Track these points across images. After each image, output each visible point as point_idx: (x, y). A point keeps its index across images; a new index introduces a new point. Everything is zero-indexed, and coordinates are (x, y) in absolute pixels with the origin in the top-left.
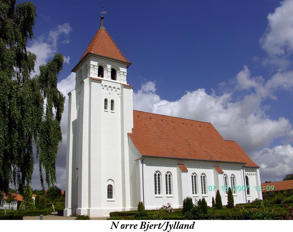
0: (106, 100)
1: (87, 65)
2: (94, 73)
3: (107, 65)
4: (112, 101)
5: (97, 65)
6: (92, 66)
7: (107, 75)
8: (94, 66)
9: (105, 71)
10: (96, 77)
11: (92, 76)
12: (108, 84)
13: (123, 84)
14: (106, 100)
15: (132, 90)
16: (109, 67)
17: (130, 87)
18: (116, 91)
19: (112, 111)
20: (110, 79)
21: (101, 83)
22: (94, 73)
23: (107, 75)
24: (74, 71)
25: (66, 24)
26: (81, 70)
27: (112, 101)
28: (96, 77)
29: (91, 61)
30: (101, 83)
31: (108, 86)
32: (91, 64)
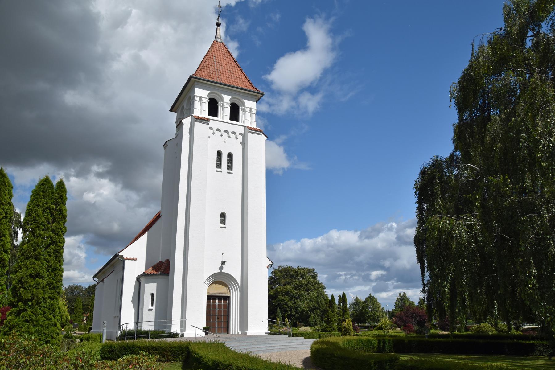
0: (219, 154)
1: (190, 98)
2: (201, 109)
3: (223, 95)
4: (230, 155)
5: (206, 97)
6: (197, 99)
7: (224, 112)
8: (201, 98)
9: (219, 107)
10: (205, 115)
11: (196, 113)
12: (223, 127)
13: (248, 127)
14: (219, 154)
15: (263, 138)
16: (227, 99)
17: (260, 131)
18: (221, 135)
19: (230, 171)
20: (227, 118)
21: (208, 124)
22: (201, 109)
23: (224, 112)
24: (173, 110)
25: (225, 19)
26: (183, 107)
27: (230, 155)
28: (205, 115)
29: (196, 89)
30: (208, 124)
31: (215, 129)
32: (195, 95)
